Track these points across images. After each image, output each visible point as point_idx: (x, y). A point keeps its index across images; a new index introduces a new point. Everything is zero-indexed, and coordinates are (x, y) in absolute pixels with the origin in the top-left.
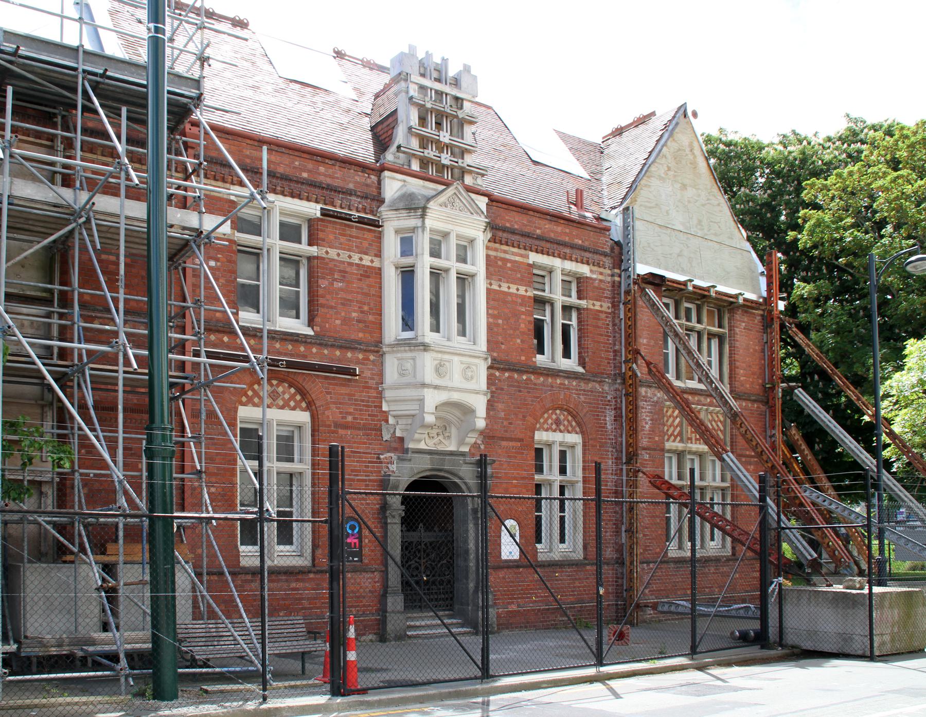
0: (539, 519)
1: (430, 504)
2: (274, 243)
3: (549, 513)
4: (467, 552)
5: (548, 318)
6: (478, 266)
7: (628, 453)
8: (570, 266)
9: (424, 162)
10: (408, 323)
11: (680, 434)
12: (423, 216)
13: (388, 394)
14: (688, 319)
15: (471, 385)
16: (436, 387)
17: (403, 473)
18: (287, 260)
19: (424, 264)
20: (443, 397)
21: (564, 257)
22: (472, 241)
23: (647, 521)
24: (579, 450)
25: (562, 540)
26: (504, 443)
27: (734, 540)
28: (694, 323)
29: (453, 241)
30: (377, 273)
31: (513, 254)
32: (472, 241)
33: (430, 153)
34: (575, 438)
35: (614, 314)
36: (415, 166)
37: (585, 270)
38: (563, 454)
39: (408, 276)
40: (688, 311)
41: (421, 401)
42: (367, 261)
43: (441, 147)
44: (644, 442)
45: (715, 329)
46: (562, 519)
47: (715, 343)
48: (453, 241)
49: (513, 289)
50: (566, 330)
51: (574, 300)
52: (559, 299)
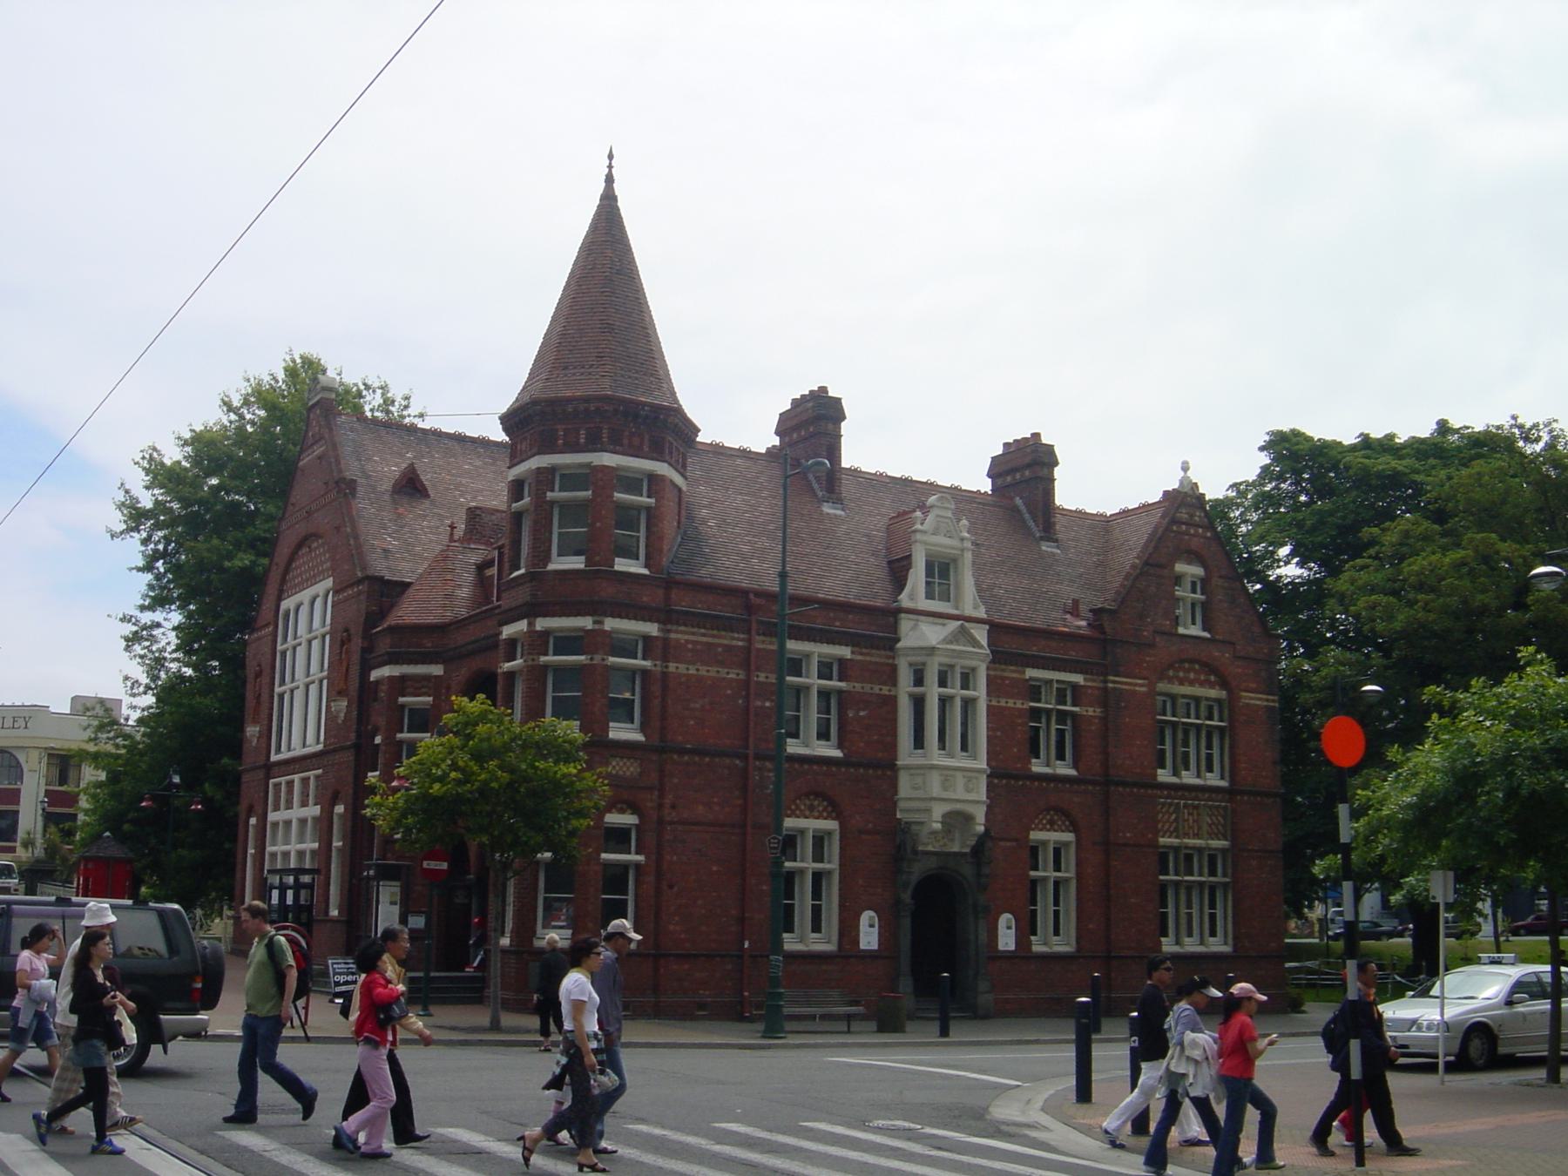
0: (1034, 913)
2: (813, 681)
3: (1044, 909)
5: (1043, 725)
6: (980, 691)
10: (919, 742)
11: (1176, 829)
13: (901, 805)
18: (824, 695)
19: (933, 692)
20: (947, 807)
22: (974, 669)
25: (1057, 933)
26: (1002, 844)
29: (958, 670)
30: (892, 702)
31: (1010, 673)
32: (974, 669)
38: (1057, 852)
39: (919, 703)
41: (928, 811)
42: (885, 690)
46: (1056, 913)
48: (958, 670)
49: (1011, 704)
50: (1061, 733)
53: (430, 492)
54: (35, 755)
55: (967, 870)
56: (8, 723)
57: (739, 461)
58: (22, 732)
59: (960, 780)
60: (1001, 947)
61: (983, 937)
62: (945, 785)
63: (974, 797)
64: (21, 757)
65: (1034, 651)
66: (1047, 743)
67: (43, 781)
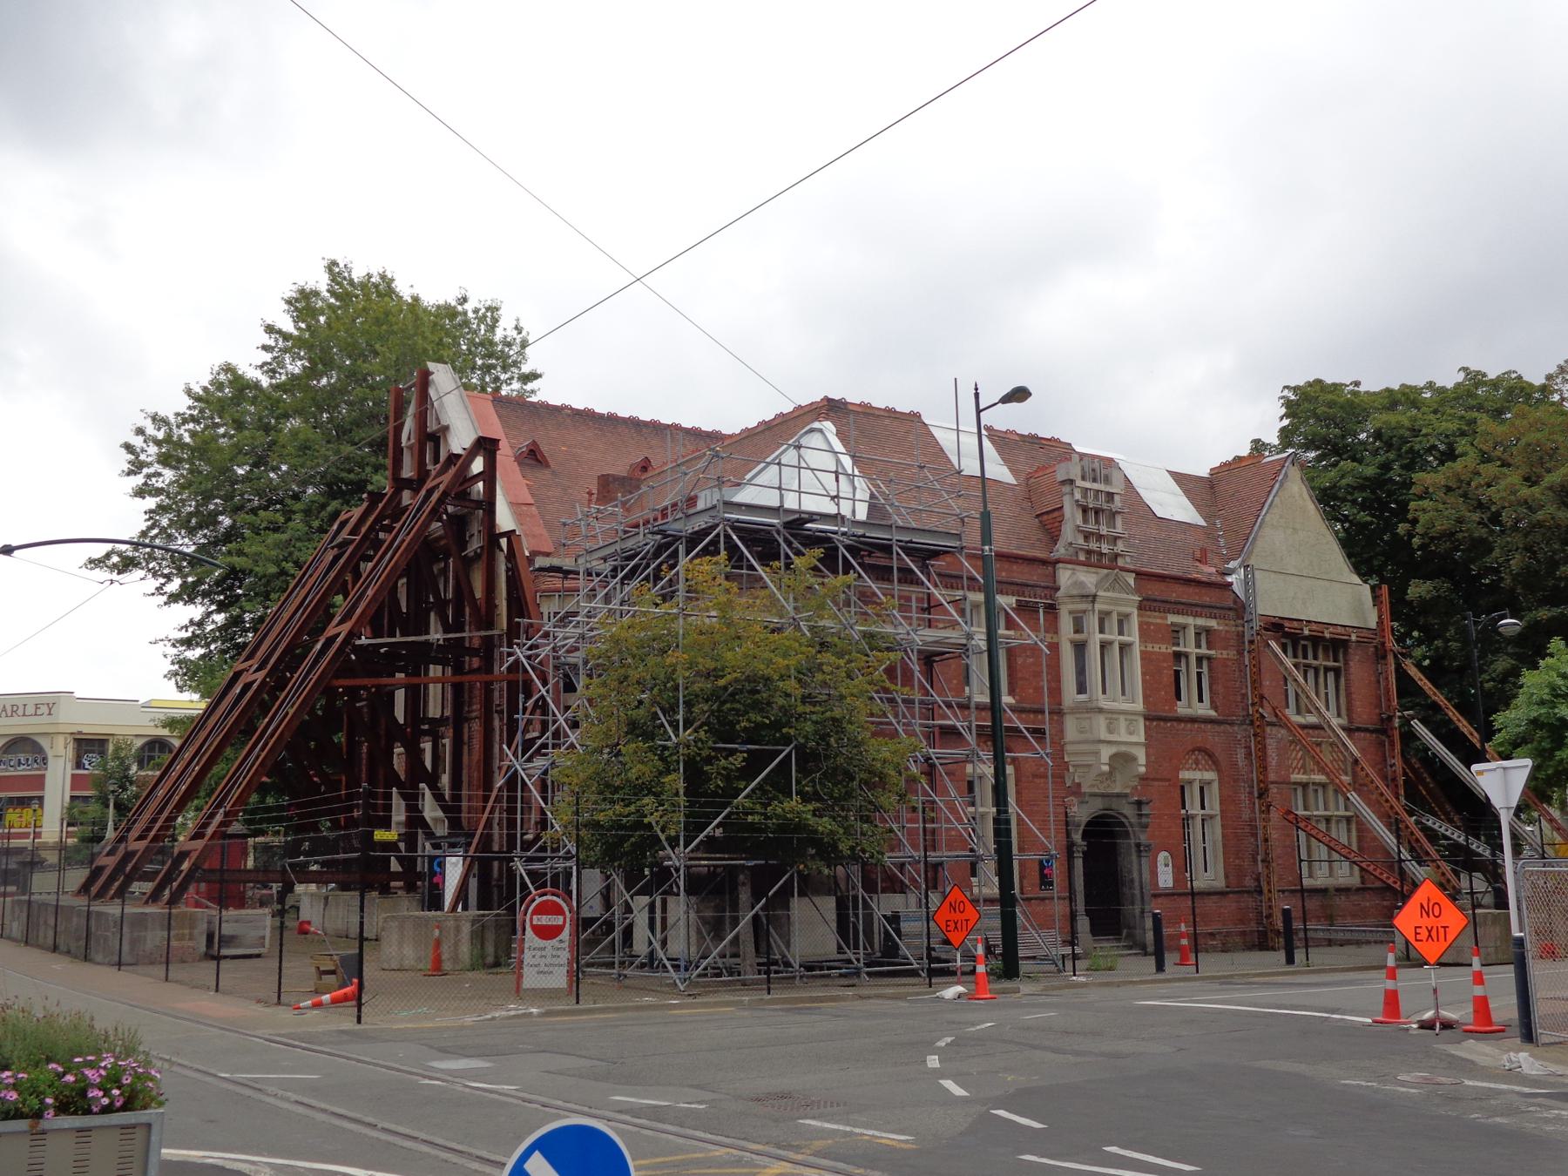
1: (1104, 845)
4: (1132, 881)
5: (1183, 668)
6: (1133, 636)
7: (1260, 789)
8: (1201, 622)
9: (1089, 552)
10: (1081, 688)
11: (1303, 767)
12: (1093, 602)
13: (1069, 748)
14: (1305, 657)
15: (1134, 739)
16: (1109, 742)
17: (1082, 813)
20: (1113, 750)
21: (1196, 615)
22: (1127, 616)
23: (1279, 851)
24: (1216, 785)
27: (1362, 869)
28: (1310, 661)
31: (1155, 619)
32: (1127, 616)
33: (1093, 545)
34: (1210, 775)
35: (1240, 662)
36: (1082, 557)
37: (1213, 623)
40: (1305, 647)
41: (1097, 753)
43: (1100, 537)
44: (1272, 776)
45: (1331, 664)
47: (1331, 676)
51: (1204, 651)
52: (1192, 650)
53: (552, 464)
54: (60, 740)
55: (1129, 811)
56: (30, 710)
57: (887, 422)
58: (45, 719)
59: (1122, 723)
60: (1161, 885)
61: (1146, 876)
62: (1109, 729)
63: (1133, 736)
64: (44, 743)
65: (1173, 597)
66: (1188, 686)
67: (69, 766)
